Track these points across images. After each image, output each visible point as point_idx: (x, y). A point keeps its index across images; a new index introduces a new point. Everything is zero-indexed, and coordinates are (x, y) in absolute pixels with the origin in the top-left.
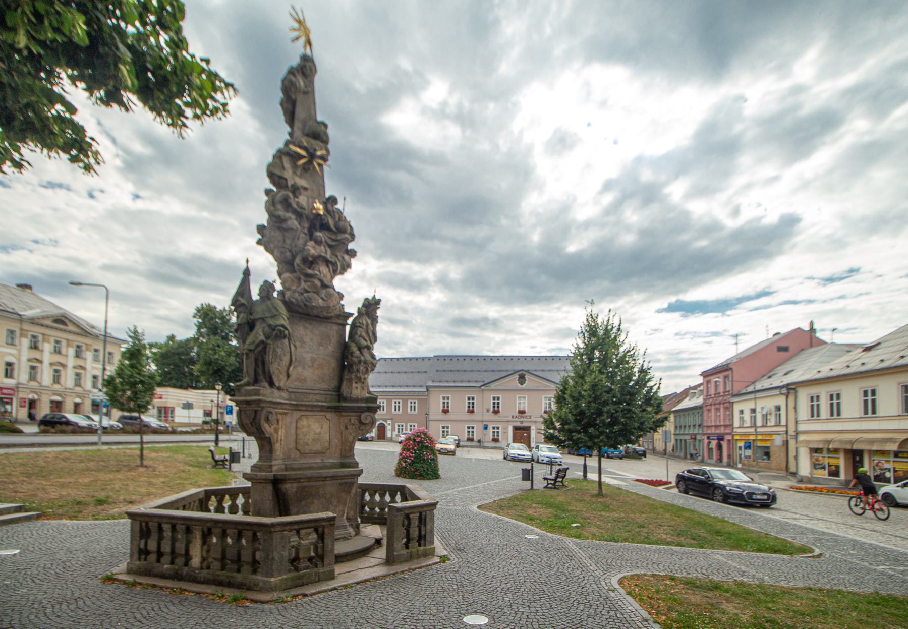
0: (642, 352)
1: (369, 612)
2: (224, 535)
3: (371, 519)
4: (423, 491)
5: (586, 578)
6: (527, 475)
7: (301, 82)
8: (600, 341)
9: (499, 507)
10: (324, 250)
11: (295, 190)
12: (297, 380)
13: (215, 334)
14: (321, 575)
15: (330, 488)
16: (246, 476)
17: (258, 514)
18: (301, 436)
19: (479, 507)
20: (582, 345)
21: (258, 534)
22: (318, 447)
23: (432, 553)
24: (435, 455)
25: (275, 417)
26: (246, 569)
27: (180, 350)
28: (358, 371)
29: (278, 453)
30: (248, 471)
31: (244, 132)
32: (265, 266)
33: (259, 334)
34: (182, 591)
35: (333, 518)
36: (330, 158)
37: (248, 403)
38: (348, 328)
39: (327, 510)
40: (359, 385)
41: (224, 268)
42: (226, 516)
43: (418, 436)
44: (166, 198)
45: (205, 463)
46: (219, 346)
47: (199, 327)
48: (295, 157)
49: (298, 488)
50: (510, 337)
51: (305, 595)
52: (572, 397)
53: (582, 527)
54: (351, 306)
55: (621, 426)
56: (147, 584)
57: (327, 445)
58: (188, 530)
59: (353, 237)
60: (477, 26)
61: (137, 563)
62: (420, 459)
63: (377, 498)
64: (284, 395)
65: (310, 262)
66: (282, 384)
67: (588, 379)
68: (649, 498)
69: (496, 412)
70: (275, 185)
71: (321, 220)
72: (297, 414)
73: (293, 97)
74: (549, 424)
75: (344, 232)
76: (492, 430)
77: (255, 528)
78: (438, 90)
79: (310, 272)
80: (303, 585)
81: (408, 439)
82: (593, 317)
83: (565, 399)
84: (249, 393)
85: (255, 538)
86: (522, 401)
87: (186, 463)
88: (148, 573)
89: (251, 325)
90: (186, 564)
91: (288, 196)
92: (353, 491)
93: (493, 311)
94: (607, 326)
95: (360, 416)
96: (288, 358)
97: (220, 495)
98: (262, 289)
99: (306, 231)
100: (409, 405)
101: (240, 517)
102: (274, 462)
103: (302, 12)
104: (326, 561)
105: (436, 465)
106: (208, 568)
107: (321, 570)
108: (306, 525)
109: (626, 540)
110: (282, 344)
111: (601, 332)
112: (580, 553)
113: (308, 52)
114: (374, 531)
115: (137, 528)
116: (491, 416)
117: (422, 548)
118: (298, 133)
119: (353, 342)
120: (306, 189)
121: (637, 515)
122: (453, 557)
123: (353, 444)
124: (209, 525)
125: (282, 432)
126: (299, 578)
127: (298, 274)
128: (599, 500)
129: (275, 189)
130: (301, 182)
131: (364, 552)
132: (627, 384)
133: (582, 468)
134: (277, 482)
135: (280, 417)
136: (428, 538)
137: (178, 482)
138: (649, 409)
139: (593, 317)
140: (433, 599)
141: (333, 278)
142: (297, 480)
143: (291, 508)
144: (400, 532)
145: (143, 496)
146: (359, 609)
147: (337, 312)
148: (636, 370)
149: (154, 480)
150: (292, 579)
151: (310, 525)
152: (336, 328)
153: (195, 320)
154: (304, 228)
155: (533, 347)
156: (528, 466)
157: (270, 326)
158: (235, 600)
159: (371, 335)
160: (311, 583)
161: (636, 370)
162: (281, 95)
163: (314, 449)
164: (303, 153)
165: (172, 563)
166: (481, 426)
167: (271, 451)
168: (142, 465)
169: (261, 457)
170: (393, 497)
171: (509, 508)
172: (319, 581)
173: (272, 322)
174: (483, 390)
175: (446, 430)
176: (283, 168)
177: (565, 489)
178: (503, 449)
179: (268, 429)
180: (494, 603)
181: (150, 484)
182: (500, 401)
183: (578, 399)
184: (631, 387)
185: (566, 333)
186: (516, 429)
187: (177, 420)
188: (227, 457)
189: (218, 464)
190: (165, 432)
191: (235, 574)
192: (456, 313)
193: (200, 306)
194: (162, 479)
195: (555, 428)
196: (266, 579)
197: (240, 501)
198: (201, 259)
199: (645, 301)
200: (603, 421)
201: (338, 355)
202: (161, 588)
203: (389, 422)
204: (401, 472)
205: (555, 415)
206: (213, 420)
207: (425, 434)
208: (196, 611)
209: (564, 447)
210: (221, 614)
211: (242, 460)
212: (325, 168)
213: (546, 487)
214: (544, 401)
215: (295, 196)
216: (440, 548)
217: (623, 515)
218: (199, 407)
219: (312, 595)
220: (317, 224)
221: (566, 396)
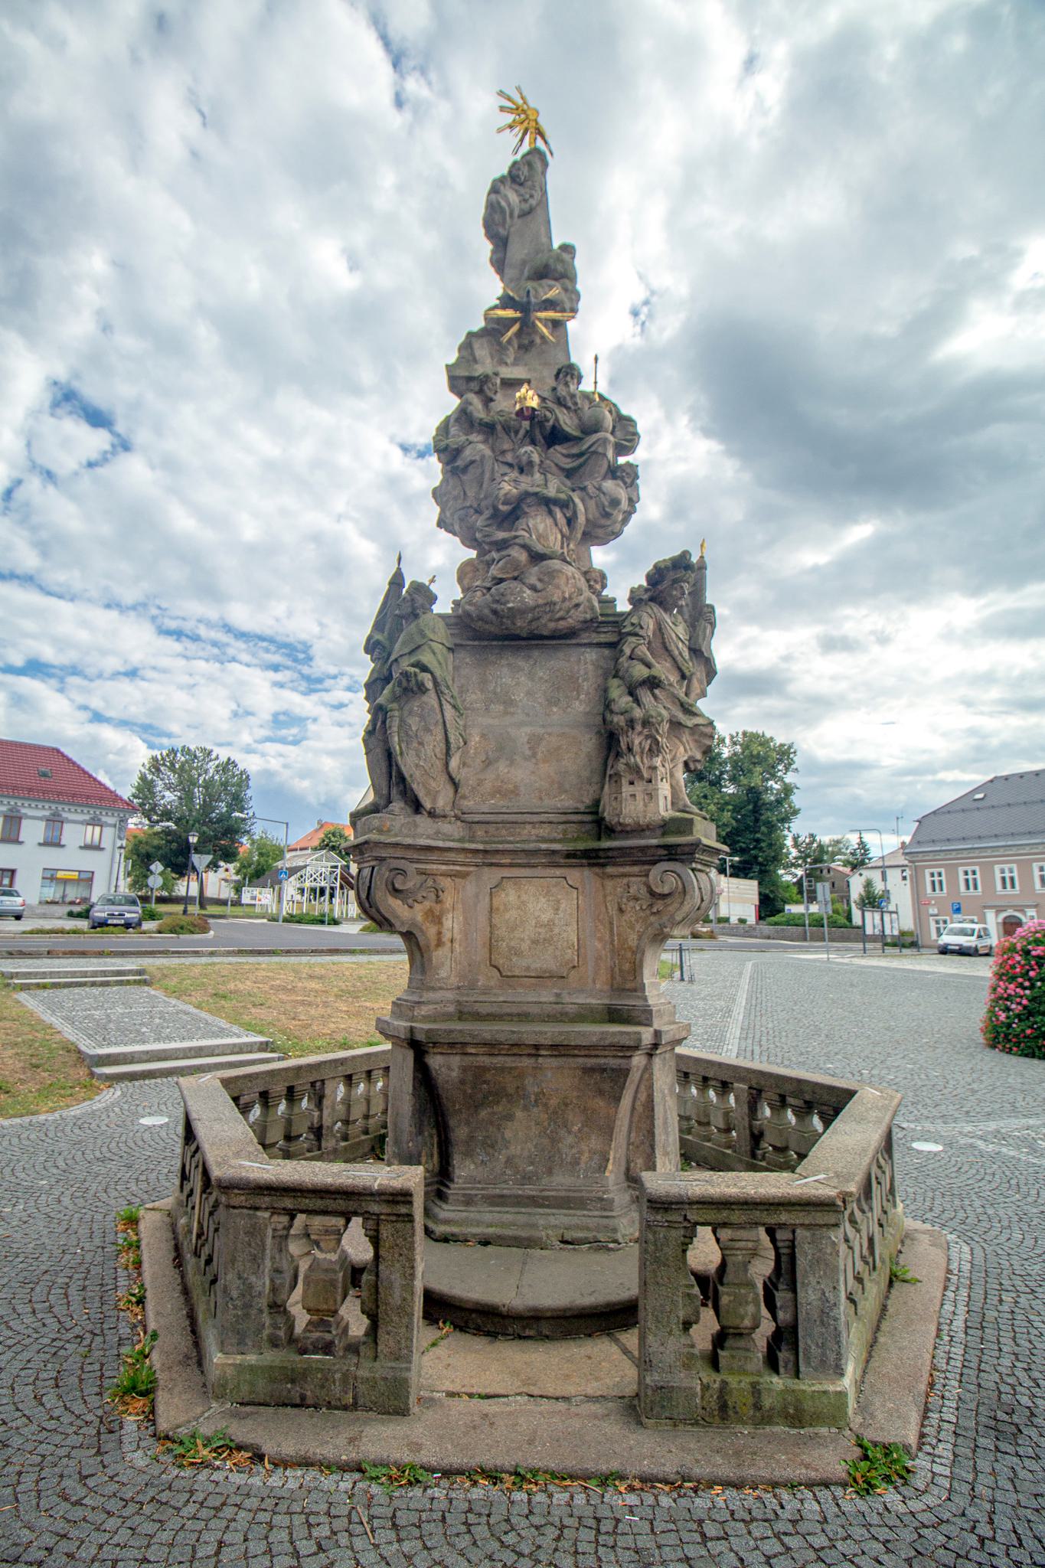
14: (362, 1388)
18: (502, 932)
22: (545, 961)
29: (443, 973)
40: (639, 788)
49: (464, 1069)
57: (570, 954)
72: (491, 876)
96: (440, 737)
107: (362, 1373)
108: (319, 1204)
117: (777, 1382)
126: (294, 1377)
135: (446, 883)
150: (273, 1374)
160: (329, 1406)
172: (355, 1406)
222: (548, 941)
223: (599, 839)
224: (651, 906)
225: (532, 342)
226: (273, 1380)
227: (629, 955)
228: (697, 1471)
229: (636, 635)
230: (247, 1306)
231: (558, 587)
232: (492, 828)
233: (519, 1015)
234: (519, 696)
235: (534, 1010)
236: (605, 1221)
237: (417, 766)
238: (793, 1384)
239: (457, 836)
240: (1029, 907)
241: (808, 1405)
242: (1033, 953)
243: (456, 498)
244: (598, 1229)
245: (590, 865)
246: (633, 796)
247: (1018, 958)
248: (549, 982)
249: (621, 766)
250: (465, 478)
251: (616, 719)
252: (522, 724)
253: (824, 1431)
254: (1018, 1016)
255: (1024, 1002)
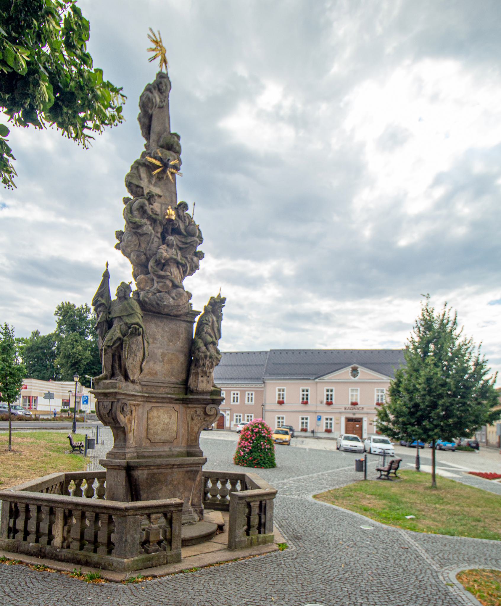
0: (477, 345)
1: (214, 596)
2: (83, 517)
3: (214, 506)
4: (262, 479)
5: (423, 571)
6: (361, 466)
7: (157, 98)
8: (435, 334)
9: (334, 497)
10: (175, 253)
11: (151, 197)
12: (150, 373)
13: (74, 330)
15: (177, 475)
16: (102, 463)
17: (112, 498)
18: (151, 426)
19: (315, 497)
20: (417, 339)
21: (113, 517)
22: (166, 436)
23: (271, 540)
24: (271, 445)
25: (129, 408)
26: (102, 549)
27: (44, 344)
28: (204, 365)
29: (131, 442)
30: (105, 458)
31: (111, 150)
32: (123, 271)
33: (116, 332)
34: (45, 568)
35: (181, 505)
36: (182, 167)
37: (105, 395)
38: (195, 325)
39: (174, 496)
40: (205, 379)
41: (81, 271)
42: (83, 500)
43: (256, 427)
44: (29, 206)
45: (64, 448)
46: (76, 341)
47: (60, 325)
48: (150, 167)
49: (148, 474)
50: (342, 331)
51: (154, 577)
52: (407, 390)
53: (417, 519)
54: (199, 305)
55: (456, 419)
56: (14, 560)
57: (174, 434)
58: (52, 512)
59: (201, 240)
60: (310, 28)
61: (7, 540)
62: (258, 449)
63: (219, 485)
64: (138, 387)
65: (162, 264)
66: (135, 378)
67: (422, 373)
68: (484, 492)
69: (329, 404)
70: (132, 193)
71: (173, 224)
72: (148, 406)
73: (150, 112)
74: (383, 416)
75: (193, 235)
76: (325, 421)
77: (111, 512)
78: (272, 94)
79: (162, 273)
80: (152, 567)
81: (247, 429)
82: (428, 311)
83: (399, 392)
84: (107, 386)
85: (110, 520)
86: (354, 393)
87: (47, 448)
88: (15, 550)
89: (109, 324)
90: (49, 543)
91: (144, 204)
92: (198, 479)
93: (325, 306)
94: (442, 320)
95: (205, 408)
96: (142, 353)
97: (78, 478)
98: (119, 290)
99: (159, 235)
100: (247, 396)
101: (95, 500)
102: (128, 450)
103: (159, 32)
104: (174, 545)
105: (273, 455)
106: (68, 547)
107: (169, 554)
109: (461, 534)
110: (138, 340)
111: (436, 326)
112: (417, 546)
113: (164, 71)
114: (216, 517)
115: (8, 509)
116: (324, 408)
117: (262, 535)
118: (153, 145)
119: (200, 338)
120: (160, 196)
121: (473, 509)
122: (291, 544)
123: (198, 433)
124: (70, 507)
125: (135, 422)
126: (150, 560)
127: (151, 276)
128: (433, 492)
129: (132, 197)
130: (156, 190)
131: (207, 537)
132: (462, 377)
133: (415, 460)
134: (129, 469)
135: (133, 408)
136: (267, 525)
137: (41, 465)
138: (485, 402)
139: (428, 311)
140: (273, 586)
141: (182, 279)
142: (148, 467)
143: (142, 493)
144: (242, 520)
145: (11, 478)
146: (204, 593)
147: (185, 310)
148: (471, 363)
149: (20, 464)
150: (143, 560)
151: (160, 510)
152: (184, 325)
153: (57, 318)
154: (157, 232)
155: (364, 341)
156: (361, 457)
157: (126, 324)
158: (92, 578)
159: (216, 331)
160: (160, 565)
161: (471, 363)
162: (139, 111)
163: (163, 438)
164: (158, 163)
165: (37, 541)
166: (315, 417)
167: (125, 440)
168: (10, 450)
169: (115, 446)
170: (234, 484)
171: (344, 498)
172: (167, 563)
173: (128, 321)
174: (317, 383)
175: (281, 420)
176: (140, 178)
177: (398, 480)
178: (336, 439)
179: (122, 419)
180: (332, 593)
181: (17, 467)
182: (333, 393)
183: (412, 392)
184: (467, 380)
185: (400, 327)
186: (349, 420)
187: (39, 408)
188: (84, 443)
189: (75, 449)
190: (30, 419)
191: (92, 554)
192: (289, 307)
193: (61, 306)
194: (27, 463)
195: (389, 421)
196: (119, 560)
197: (96, 485)
198: (58, 261)
199: (477, 293)
200: (438, 414)
201: (186, 350)
202: (27, 564)
203: (228, 412)
204: (240, 461)
205: (390, 407)
206: (71, 409)
207: (263, 425)
208: (58, 588)
209: (398, 439)
210: (79, 591)
211: (96, 446)
212: (177, 176)
213: (379, 478)
214: (376, 394)
215: (150, 204)
216: (277, 534)
217: (457, 508)
218: (58, 397)
219: (160, 576)
220: (169, 228)
221: (400, 389)
222: (167, 430)
223: (186, 394)
224: (204, 418)
225: (163, 178)
226: (143, 562)
227: (194, 434)
228: (253, 554)
229: (208, 324)
230: (134, 544)
231: (182, 300)
232: (149, 388)
233: (158, 456)
234: (159, 336)
235: (163, 454)
236: (191, 517)
237: (132, 363)
238: (264, 535)
239: (139, 390)
240: (228, 410)
241: (267, 539)
242: (255, 431)
243: (135, 245)
244: (190, 519)
245: (183, 403)
246: (203, 381)
247: (250, 432)
248: (167, 444)
249: (199, 370)
250: (141, 238)
251: (200, 354)
252: (159, 348)
253: (270, 544)
254: (248, 453)
255: (250, 448)
